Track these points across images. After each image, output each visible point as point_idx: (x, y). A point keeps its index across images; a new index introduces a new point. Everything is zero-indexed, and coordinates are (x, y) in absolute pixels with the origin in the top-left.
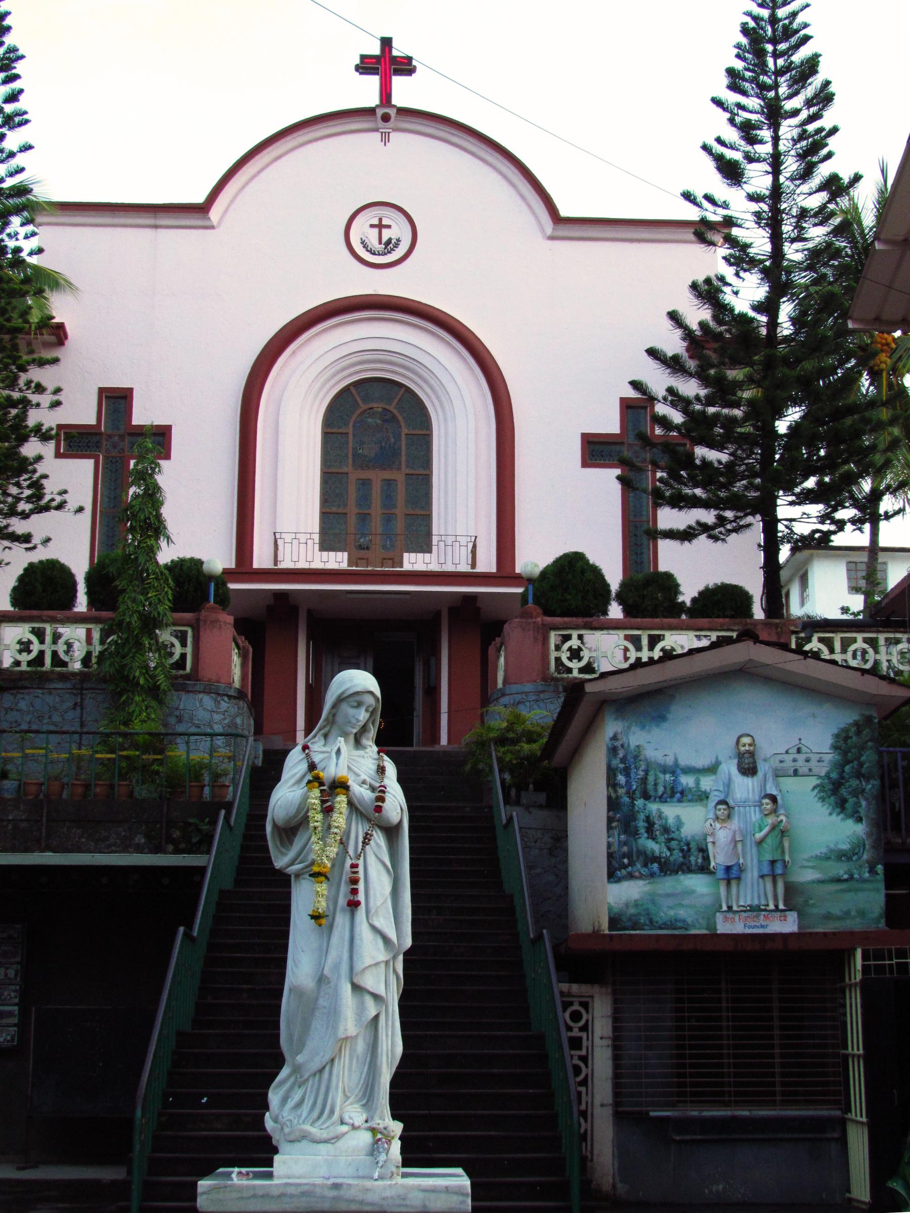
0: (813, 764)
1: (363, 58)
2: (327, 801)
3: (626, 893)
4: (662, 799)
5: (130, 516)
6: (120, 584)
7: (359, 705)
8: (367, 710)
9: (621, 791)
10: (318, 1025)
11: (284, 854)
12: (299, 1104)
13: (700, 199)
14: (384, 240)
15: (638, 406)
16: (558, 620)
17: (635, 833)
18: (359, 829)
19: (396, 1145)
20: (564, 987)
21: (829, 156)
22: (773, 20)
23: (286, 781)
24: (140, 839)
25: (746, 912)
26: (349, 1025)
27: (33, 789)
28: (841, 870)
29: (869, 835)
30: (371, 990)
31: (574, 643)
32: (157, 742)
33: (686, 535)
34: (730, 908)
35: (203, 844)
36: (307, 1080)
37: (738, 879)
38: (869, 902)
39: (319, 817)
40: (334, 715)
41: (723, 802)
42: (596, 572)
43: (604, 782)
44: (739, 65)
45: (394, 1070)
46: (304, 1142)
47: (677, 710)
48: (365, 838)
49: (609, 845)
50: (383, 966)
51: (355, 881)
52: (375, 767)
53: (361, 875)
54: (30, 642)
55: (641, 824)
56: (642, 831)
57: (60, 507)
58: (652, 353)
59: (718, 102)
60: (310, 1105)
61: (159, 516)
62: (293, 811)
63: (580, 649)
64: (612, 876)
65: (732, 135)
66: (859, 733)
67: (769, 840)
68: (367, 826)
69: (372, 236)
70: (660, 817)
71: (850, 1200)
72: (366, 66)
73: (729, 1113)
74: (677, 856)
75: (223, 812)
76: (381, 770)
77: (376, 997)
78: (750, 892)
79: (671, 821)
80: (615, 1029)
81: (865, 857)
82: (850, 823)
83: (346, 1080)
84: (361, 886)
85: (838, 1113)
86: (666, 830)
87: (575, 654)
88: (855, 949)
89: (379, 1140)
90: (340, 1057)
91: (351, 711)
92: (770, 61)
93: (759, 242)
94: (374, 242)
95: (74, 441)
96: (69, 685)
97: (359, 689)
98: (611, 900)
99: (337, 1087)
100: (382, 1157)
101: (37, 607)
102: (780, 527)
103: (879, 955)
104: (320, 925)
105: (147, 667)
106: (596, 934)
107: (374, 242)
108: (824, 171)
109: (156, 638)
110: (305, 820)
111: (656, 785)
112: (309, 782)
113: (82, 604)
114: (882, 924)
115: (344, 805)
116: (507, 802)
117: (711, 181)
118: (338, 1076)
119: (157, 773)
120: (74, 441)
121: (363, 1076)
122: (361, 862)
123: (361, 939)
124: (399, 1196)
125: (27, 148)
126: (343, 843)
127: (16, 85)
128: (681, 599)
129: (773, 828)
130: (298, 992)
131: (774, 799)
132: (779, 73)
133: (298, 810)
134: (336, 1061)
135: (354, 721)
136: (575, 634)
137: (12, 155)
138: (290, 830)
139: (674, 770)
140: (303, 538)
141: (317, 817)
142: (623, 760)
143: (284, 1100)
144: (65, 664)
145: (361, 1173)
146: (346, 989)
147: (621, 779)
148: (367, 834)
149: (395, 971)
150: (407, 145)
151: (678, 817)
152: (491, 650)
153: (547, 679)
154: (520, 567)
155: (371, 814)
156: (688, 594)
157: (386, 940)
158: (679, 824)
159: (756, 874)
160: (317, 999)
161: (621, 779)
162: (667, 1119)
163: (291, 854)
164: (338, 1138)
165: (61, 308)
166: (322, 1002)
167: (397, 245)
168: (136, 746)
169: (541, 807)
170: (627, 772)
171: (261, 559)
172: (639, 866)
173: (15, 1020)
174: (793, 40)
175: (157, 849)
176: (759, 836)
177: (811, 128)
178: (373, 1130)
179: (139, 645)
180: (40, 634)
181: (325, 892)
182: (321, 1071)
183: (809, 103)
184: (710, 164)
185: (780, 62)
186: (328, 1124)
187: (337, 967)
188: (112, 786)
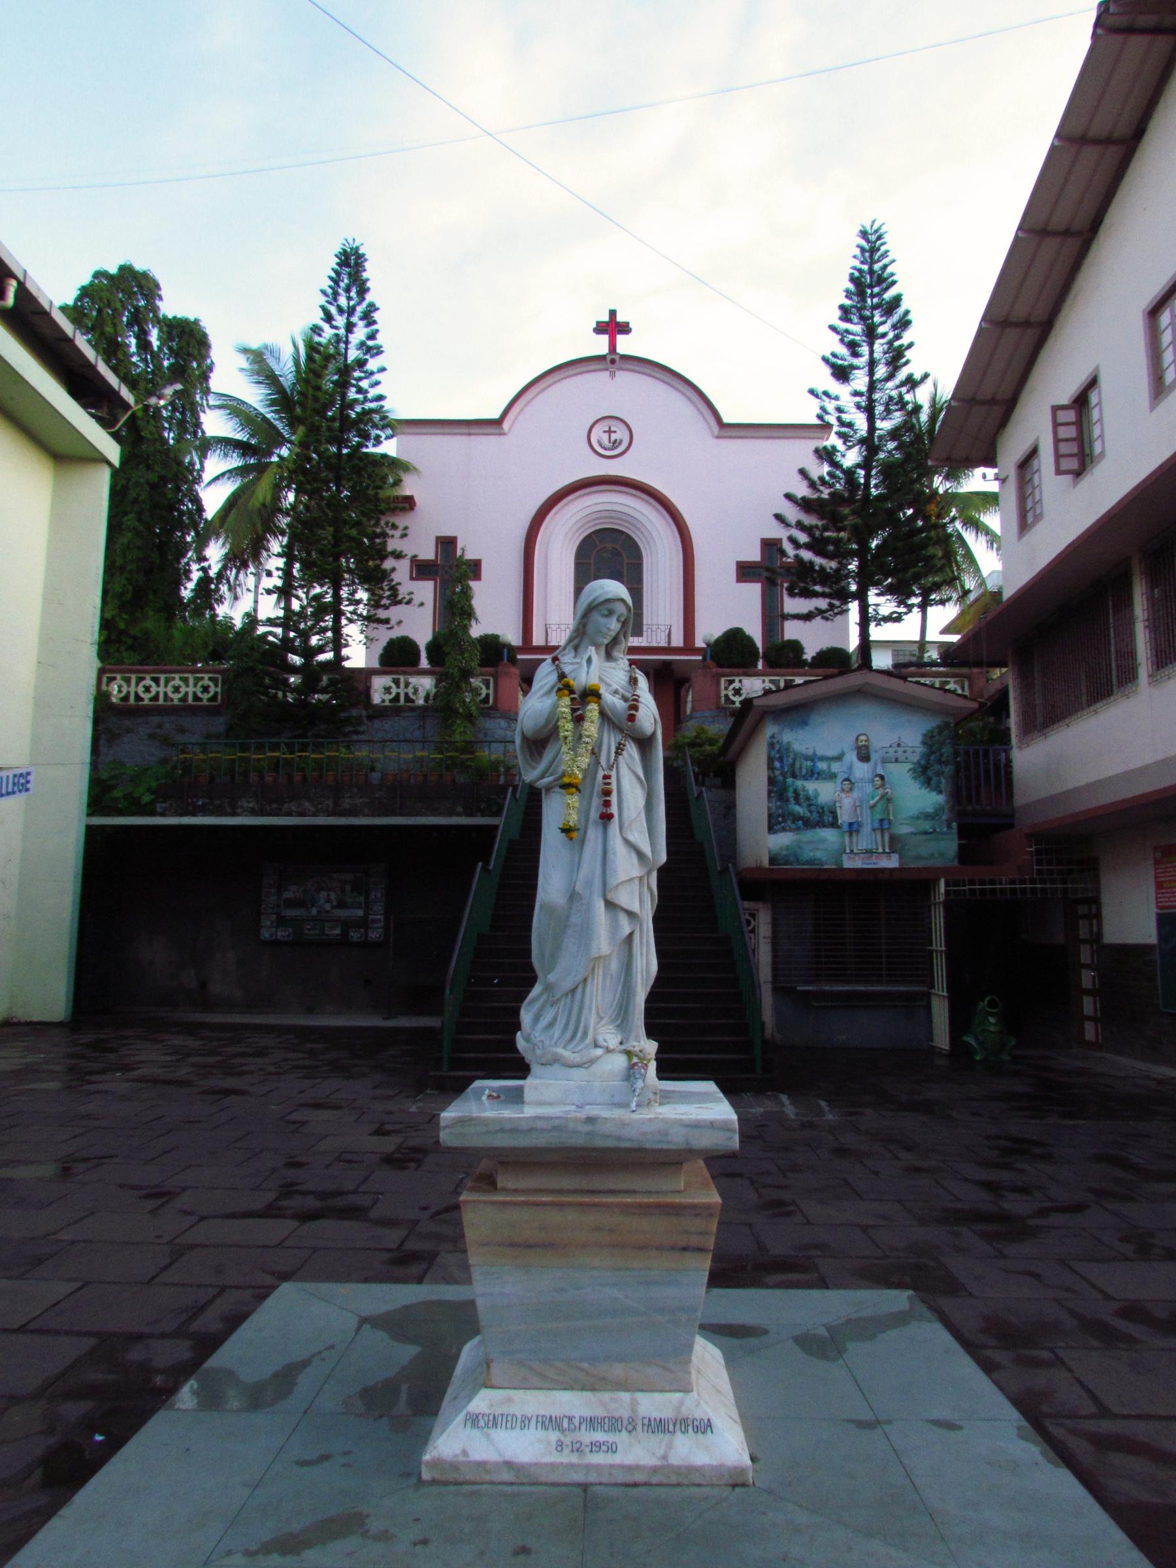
0: (908, 754)
1: (598, 323)
2: (578, 709)
3: (781, 841)
4: (805, 778)
5: (455, 609)
6: (447, 649)
7: (611, 613)
8: (618, 620)
9: (777, 773)
10: (570, 944)
11: (534, 768)
12: (551, 1025)
13: (820, 394)
14: (613, 439)
15: (770, 546)
16: (727, 670)
17: (787, 801)
18: (611, 740)
19: (653, 1066)
20: (746, 904)
21: (907, 362)
22: (871, 272)
23: (535, 693)
24: (460, 809)
25: (863, 853)
26: (603, 943)
27: (390, 778)
28: (927, 826)
29: (947, 802)
30: (625, 906)
31: (736, 685)
32: (469, 747)
33: (808, 617)
34: (852, 851)
35: (498, 813)
36: (559, 1000)
37: (857, 831)
38: (947, 847)
39: (570, 726)
40: (584, 626)
41: (847, 779)
42: (750, 640)
43: (765, 767)
44: (848, 302)
45: (649, 989)
46: (557, 1066)
47: (815, 719)
48: (618, 748)
49: (769, 809)
50: (637, 881)
51: (607, 793)
52: (627, 679)
53: (614, 787)
54: (390, 687)
55: (790, 794)
56: (792, 799)
57: (409, 603)
58: (789, 497)
59: (833, 328)
60: (564, 1022)
61: (470, 606)
62: (542, 721)
63: (740, 689)
64: (771, 829)
65: (843, 351)
66: (940, 733)
67: (879, 806)
68: (619, 737)
69: (605, 437)
70: (804, 790)
71: (933, 1047)
72: (600, 328)
73: (850, 988)
74: (815, 816)
75: (511, 789)
76: (633, 681)
77: (630, 914)
78: (864, 841)
79: (811, 792)
80: (774, 932)
81: (944, 817)
82: (934, 794)
83: (599, 999)
84: (614, 798)
85: (925, 989)
86: (808, 798)
87: (737, 692)
88: (939, 879)
89: (636, 1064)
90: (593, 979)
91: (602, 620)
92: (869, 301)
93: (860, 422)
94: (606, 442)
95: (422, 570)
96: (414, 714)
97: (609, 596)
98: (771, 845)
99: (590, 1009)
100: (639, 1084)
101: (394, 666)
102: (871, 610)
103: (956, 884)
104: (571, 839)
105: (464, 702)
106: (760, 869)
107: (606, 442)
108: (902, 375)
109: (470, 684)
110: (555, 730)
111: (801, 768)
112: (559, 690)
113: (424, 663)
114: (956, 863)
115: (596, 713)
116: (697, 784)
117: (825, 380)
118: (591, 998)
119: (470, 767)
120: (422, 570)
121: (618, 996)
122: (613, 773)
123: (615, 854)
124: (659, 1132)
125: (383, 370)
126: (595, 753)
127: (375, 327)
128: (805, 657)
129: (882, 797)
130: (550, 910)
131: (882, 777)
132: (874, 307)
133: (548, 721)
134: (589, 981)
135: (605, 630)
136: (737, 679)
137: (372, 373)
138: (538, 743)
139: (813, 758)
140: (563, 627)
141: (567, 727)
142: (779, 752)
143: (536, 1019)
144: (413, 701)
145: (616, 1100)
146: (600, 905)
147: (777, 764)
148: (620, 744)
149: (649, 888)
150: (627, 379)
151: (816, 791)
152: (683, 693)
153: (719, 708)
154: (699, 643)
155: (623, 725)
156: (809, 654)
157: (640, 855)
158: (817, 795)
159: (869, 827)
160: (568, 917)
161: (777, 764)
162: (809, 991)
163: (542, 767)
164: (592, 1062)
165: (410, 487)
166: (575, 919)
167: (620, 443)
168: (456, 751)
169: (718, 787)
170: (781, 759)
171: (538, 640)
172: (789, 823)
173: (382, 924)
174: (884, 285)
175: (471, 815)
176: (872, 802)
177: (896, 344)
178: (629, 1053)
179: (459, 687)
180: (397, 682)
181: (576, 805)
182: (573, 991)
183: (894, 327)
184: (827, 371)
185: (875, 300)
186: (582, 1046)
187: (589, 883)
188: (441, 776)
